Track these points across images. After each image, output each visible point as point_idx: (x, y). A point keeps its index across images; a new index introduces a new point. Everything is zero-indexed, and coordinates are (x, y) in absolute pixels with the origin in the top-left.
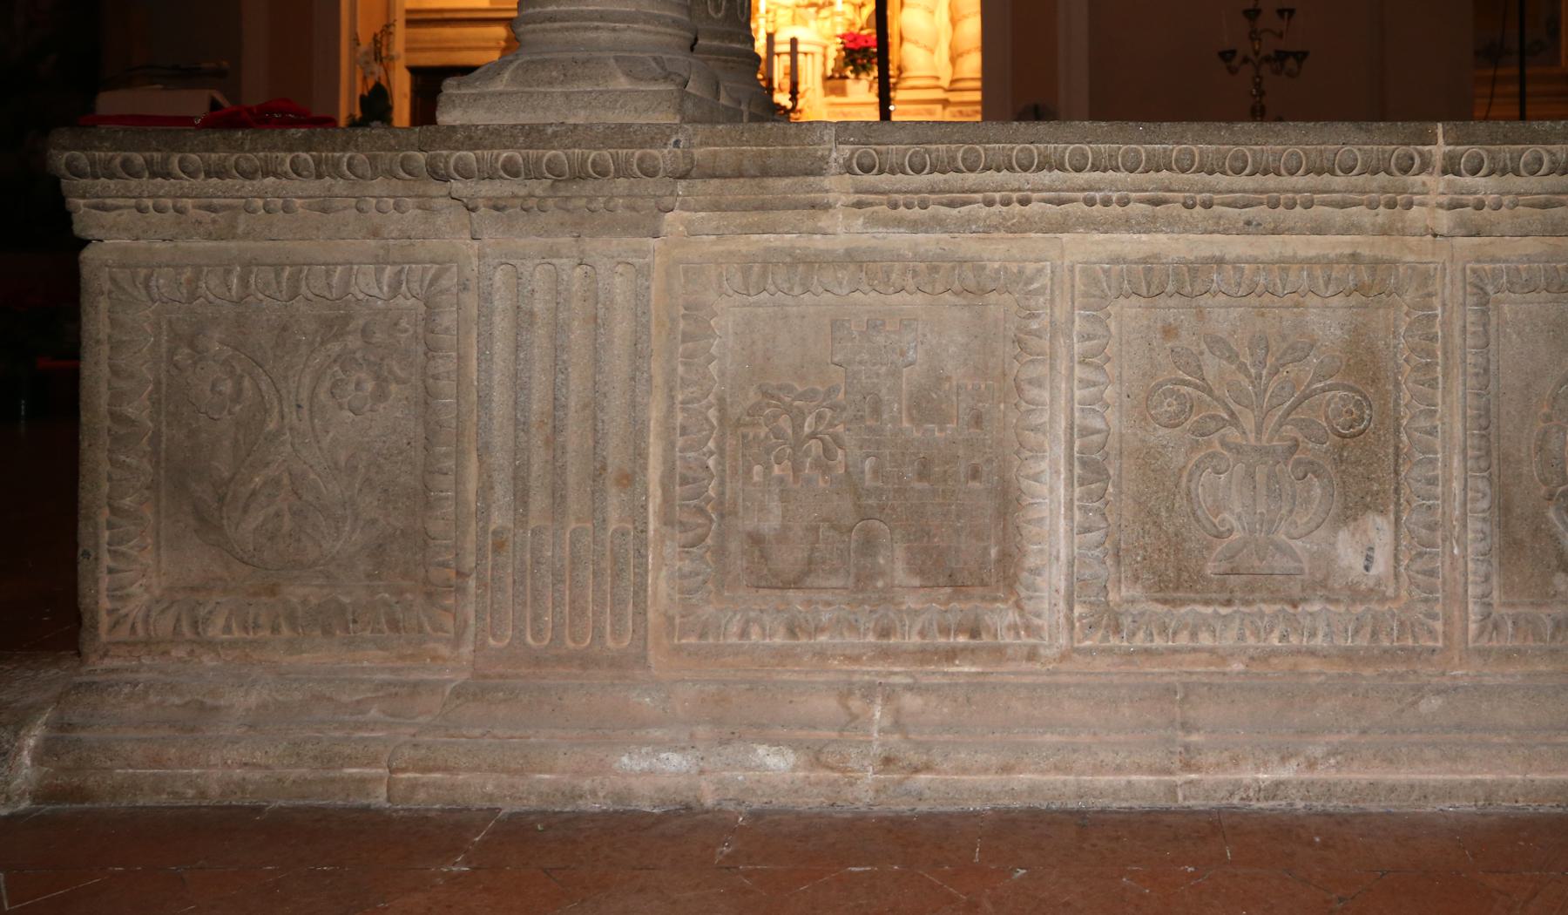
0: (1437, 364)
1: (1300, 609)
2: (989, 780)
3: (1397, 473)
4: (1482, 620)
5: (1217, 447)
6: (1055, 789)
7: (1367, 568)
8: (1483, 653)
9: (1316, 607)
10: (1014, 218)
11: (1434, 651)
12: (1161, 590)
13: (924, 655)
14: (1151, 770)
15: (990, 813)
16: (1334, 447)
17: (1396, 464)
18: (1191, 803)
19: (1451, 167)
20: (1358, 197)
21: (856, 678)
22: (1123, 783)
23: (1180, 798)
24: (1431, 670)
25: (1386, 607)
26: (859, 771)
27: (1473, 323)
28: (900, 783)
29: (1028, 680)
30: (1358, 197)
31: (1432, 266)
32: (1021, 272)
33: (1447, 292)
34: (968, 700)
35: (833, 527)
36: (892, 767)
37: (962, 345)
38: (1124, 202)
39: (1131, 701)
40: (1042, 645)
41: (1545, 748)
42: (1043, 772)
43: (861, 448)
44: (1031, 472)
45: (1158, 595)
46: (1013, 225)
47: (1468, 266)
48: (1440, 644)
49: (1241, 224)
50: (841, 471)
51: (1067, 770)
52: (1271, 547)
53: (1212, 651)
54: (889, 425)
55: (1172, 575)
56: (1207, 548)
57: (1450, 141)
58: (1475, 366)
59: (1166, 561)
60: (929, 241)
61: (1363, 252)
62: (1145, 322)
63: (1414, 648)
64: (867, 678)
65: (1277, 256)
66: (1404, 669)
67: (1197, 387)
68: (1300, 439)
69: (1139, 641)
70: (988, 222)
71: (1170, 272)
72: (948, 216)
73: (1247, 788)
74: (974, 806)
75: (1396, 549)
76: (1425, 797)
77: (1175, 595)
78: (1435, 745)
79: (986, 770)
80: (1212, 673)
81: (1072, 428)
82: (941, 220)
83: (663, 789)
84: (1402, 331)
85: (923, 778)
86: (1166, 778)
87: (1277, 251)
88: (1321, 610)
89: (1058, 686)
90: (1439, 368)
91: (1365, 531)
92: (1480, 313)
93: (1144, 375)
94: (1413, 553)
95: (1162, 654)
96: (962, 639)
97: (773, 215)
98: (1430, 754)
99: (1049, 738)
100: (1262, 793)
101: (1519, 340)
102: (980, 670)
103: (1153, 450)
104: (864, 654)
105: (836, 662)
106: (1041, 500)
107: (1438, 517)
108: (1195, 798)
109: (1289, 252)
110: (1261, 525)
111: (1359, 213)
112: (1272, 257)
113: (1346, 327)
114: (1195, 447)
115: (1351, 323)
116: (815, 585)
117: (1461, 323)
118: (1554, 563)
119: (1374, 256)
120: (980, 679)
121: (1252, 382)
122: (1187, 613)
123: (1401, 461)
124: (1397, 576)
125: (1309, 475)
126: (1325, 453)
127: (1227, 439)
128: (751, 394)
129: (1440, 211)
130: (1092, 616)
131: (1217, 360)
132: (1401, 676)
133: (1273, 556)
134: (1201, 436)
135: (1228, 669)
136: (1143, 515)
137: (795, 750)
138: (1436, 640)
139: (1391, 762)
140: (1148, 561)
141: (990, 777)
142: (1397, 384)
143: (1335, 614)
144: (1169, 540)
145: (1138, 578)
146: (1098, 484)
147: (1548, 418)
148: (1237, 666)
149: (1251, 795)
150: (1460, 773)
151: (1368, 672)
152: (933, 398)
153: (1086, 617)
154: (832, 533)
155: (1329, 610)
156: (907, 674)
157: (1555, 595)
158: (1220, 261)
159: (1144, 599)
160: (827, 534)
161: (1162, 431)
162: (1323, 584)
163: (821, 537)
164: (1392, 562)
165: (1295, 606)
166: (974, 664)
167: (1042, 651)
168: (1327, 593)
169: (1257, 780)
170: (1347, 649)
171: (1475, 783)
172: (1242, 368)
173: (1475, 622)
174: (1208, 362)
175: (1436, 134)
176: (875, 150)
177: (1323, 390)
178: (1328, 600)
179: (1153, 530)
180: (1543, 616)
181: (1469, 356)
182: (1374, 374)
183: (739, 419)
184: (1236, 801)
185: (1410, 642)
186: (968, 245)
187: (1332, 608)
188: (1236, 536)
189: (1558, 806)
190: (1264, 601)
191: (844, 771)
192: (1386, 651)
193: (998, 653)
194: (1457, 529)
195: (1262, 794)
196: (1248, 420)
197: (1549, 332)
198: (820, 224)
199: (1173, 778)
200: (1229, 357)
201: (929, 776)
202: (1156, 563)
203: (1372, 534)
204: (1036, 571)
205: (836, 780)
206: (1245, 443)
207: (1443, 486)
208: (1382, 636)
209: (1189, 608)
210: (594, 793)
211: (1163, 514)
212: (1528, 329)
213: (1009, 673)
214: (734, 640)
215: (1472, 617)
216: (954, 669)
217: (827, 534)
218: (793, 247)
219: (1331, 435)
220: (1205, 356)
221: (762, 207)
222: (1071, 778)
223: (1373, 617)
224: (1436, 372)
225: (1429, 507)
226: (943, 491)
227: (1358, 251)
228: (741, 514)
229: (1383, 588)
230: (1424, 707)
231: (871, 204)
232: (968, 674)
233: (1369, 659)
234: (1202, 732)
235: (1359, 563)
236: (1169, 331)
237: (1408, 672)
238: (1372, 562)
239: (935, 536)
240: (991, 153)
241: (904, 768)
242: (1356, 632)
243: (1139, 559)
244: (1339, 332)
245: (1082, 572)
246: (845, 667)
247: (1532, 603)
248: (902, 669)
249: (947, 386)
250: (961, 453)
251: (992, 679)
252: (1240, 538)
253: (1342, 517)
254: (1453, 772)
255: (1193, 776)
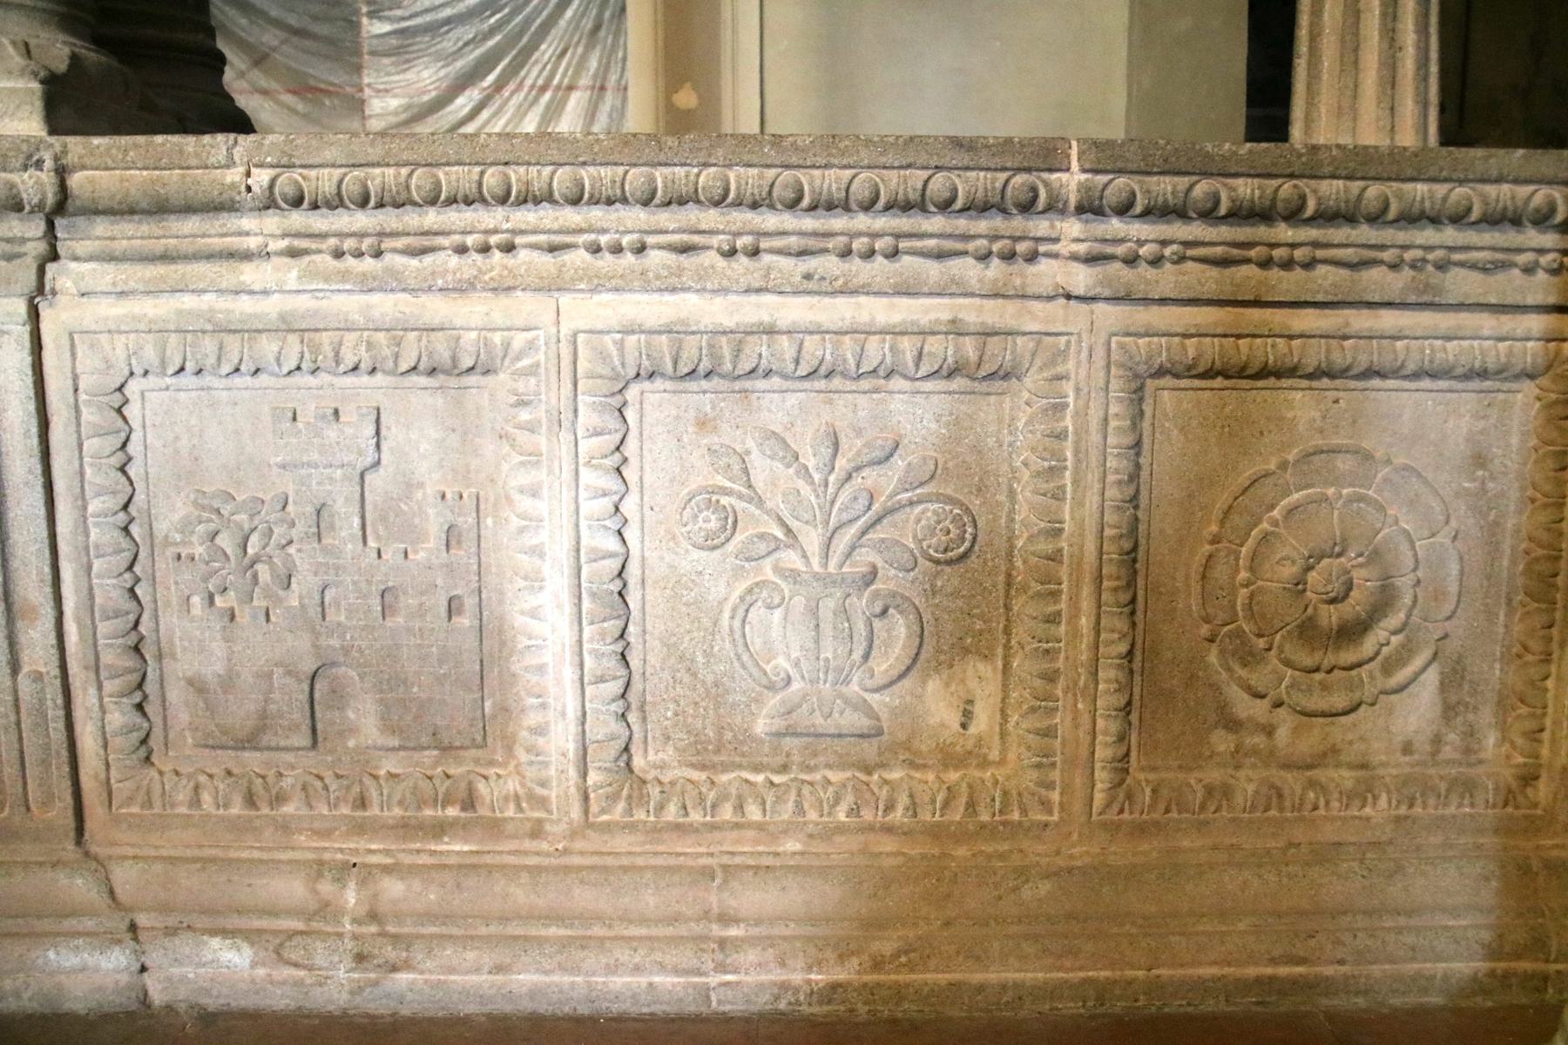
0: (1065, 468)
1: (876, 777)
2: (482, 979)
3: (1007, 608)
4: (1110, 789)
5: (770, 574)
6: (561, 992)
7: (964, 726)
8: (1113, 828)
9: (895, 775)
10: (492, 269)
11: (1046, 825)
12: (698, 753)
13: (406, 829)
14: (677, 971)
15: (484, 1019)
16: (925, 574)
17: (1007, 595)
18: (727, 1008)
19: (1089, 208)
20: (959, 246)
21: (327, 856)
22: (644, 985)
23: (714, 1004)
24: (1040, 848)
25: (989, 774)
26: (327, 969)
27: (1117, 415)
28: (376, 983)
29: (532, 861)
30: (959, 246)
31: (1063, 339)
32: (507, 346)
33: (1083, 373)
34: (458, 885)
35: (289, 673)
36: (365, 964)
37: (436, 440)
38: (641, 249)
39: (657, 888)
40: (548, 820)
41: (1178, 938)
42: (546, 973)
43: (316, 574)
44: (527, 606)
45: (694, 759)
46: (491, 279)
47: (1114, 339)
48: (1056, 817)
49: (799, 278)
50: (296, 603)
51: (576, 970)
52: (838, 701)
53: (760, 827)
54: (350, 546)
55: (711, 734)
56: (756, 701)
57: (1087, 166)
58: (1117, 471)
59: (704, 718)
60: (386, 305)
61: (967, 318)
62: (674, 412)
63: (1020, 823)
64: (339, 856)
65: (847, 322)
66: (1006, 848)
67: (740, 497)
68: (879, 565)
69: (672, 813)
70: (458, 275)
71: (704, 344)
72: (406, 267)
73: (797, 990)
74: (470, 1008)
75: (1003, 700)
76: (1020, 998)
77: (716, 759)
78: (1036, 938)
79: (478, 970)
80: (760, 854)
81: (578, 550)
82: (398, 273)
83: (100, 989)
84: (1020, 425)
85: (403, 977)
86: (696, 979)
87: (848, 316)
88: (902, 779)
89: (567, 869)
90: (1068, 473)
91: (963, 681)
92: (1127, 402)
93: (672, 481)
94: (1025, 707)
95: (697, 831)
96: (452, 812)
97: (181, 268)
98: (1029, 948)
99: (553, 931)
100: (815, 996)
101: (1182, 438)
102: (474, 848)
103: (685, 578)
104: (336, 829)
105: (303, 838)
106: (540, 642)
107: (1060, 664)
108: (732, 1004)
109: (864, 317)
110: (826, 673)
111: (966, 269)
112: (840, 324)
113: (944, 419)
114: (738, 572)
115: (951, 414)
116: (273, 744)
117: (1101, 414)
118: (1213, 717)
119: (982, 323)
120: (474, 860)
121: (815, 491)
122: (730, 782)
123: (1013, 592)
124: (1003, 734)
125: (891, 611)
126: (913, 582)
127: (781, 565)
128: (180, 504)
129: (1076, 264)
130: (610, 785)
131: (769, 461)
132: (1002, 856)
133: (842, 713)
134: (747, 560)
135: (781, 849)
136: (672, 660)
137: (252, 944)
138: (1050, 813)
139: (978, 959)
140: (680, 718)
141: (484, 977)
142: (1012, 494)
143: (920, 781)
144: (707, 692)
145: (669, 738)
146: (612, 622)
147: (1215, 540)
148: (792, 845)
149: (802, 998)
150: (1068, 970)
151: (962, 851)
152: (402, 511)
153: (602, 787)
154: (288, 680)
155: (911, 778)
156: (387, 852)
157: (1211, 757)
158: (771, 331)
159: (676, 764)
160: (283, 681)
161: (696, 554)
162: (907, 746)
163: (276, 685)
164: (998, 717)
165: (870, 773)
166: (466, 842)
167: (548, 827)
168: (911, 757)
169: (809, 982)
170: (938, 825)
171: (1085, 981)
172: (805, 472)
173: (1103, 791)
174: (756, 464)
175: (1068, 156)
176: (300, 174)
177: (911, 503)
178: (912, 765)
179: (687, 679)
180: (1193, 782)
181: (1109, 458)
182: (981, 480)
183: (166, 537)
184: (782, 1005)
185: (1016, 816)
186: (436, 308)
187: (918, 775)
188: (796, 685)
189: (1189, 1004)
190: (829, 766)
191: (310, 968)
192: (983, 826)
193: (495, 827)
194: (1083, 677)
195: (815, 997)
196: (812, 539)
197: (1223, 427)
198: (242, 278)
199: (703, 979)
200: (785, 457)
201: (411, 976)
202: (690, 720)
203: (973, 684)
204: (540, 730)
205: (302, 979)
206: (804, 569)
207: (1068, 623)
208: (981, 808)
209: (733, 775)
210: (17, 995)
211: (700, 659)
212: (1194, 423)
213: (510, 853)
214: (183, 810)
215: (1099, 786)
216: (440, 848)
217: (283, 681)
218: (212, 310)
219: (921, 560)
220: (753, 456)
221: (166, 257)
222: (579, 979)
223: (970, 786)
224: (1063, 477)
225: (1047, 651)
226: (420, 630)
227: (960, 316)
228: (179, 656)
229: (985, 750)
230: (1027, 893)
231: (306, 252)
232: (458, 853)
233: (961, 835)
234: (742, 925)
235: (954, 720)
236: (704, 423)
237: (1011, 851)
238: (971, 719)
239: (413, 685)
240: (454, 177)
241: (379, 966)
242: (946, 804)
243: (669, 714)
244: (933, 426)
245: (595, 731)
246: (315, 844)
247: (1180, 767)
248: (381, 847)
249: (419, 495)
250: (439, 582)
251: (488, 859)
252: (798, 690)
253: (934, 663)
254: (1059, 969)
255: (729, 978)
